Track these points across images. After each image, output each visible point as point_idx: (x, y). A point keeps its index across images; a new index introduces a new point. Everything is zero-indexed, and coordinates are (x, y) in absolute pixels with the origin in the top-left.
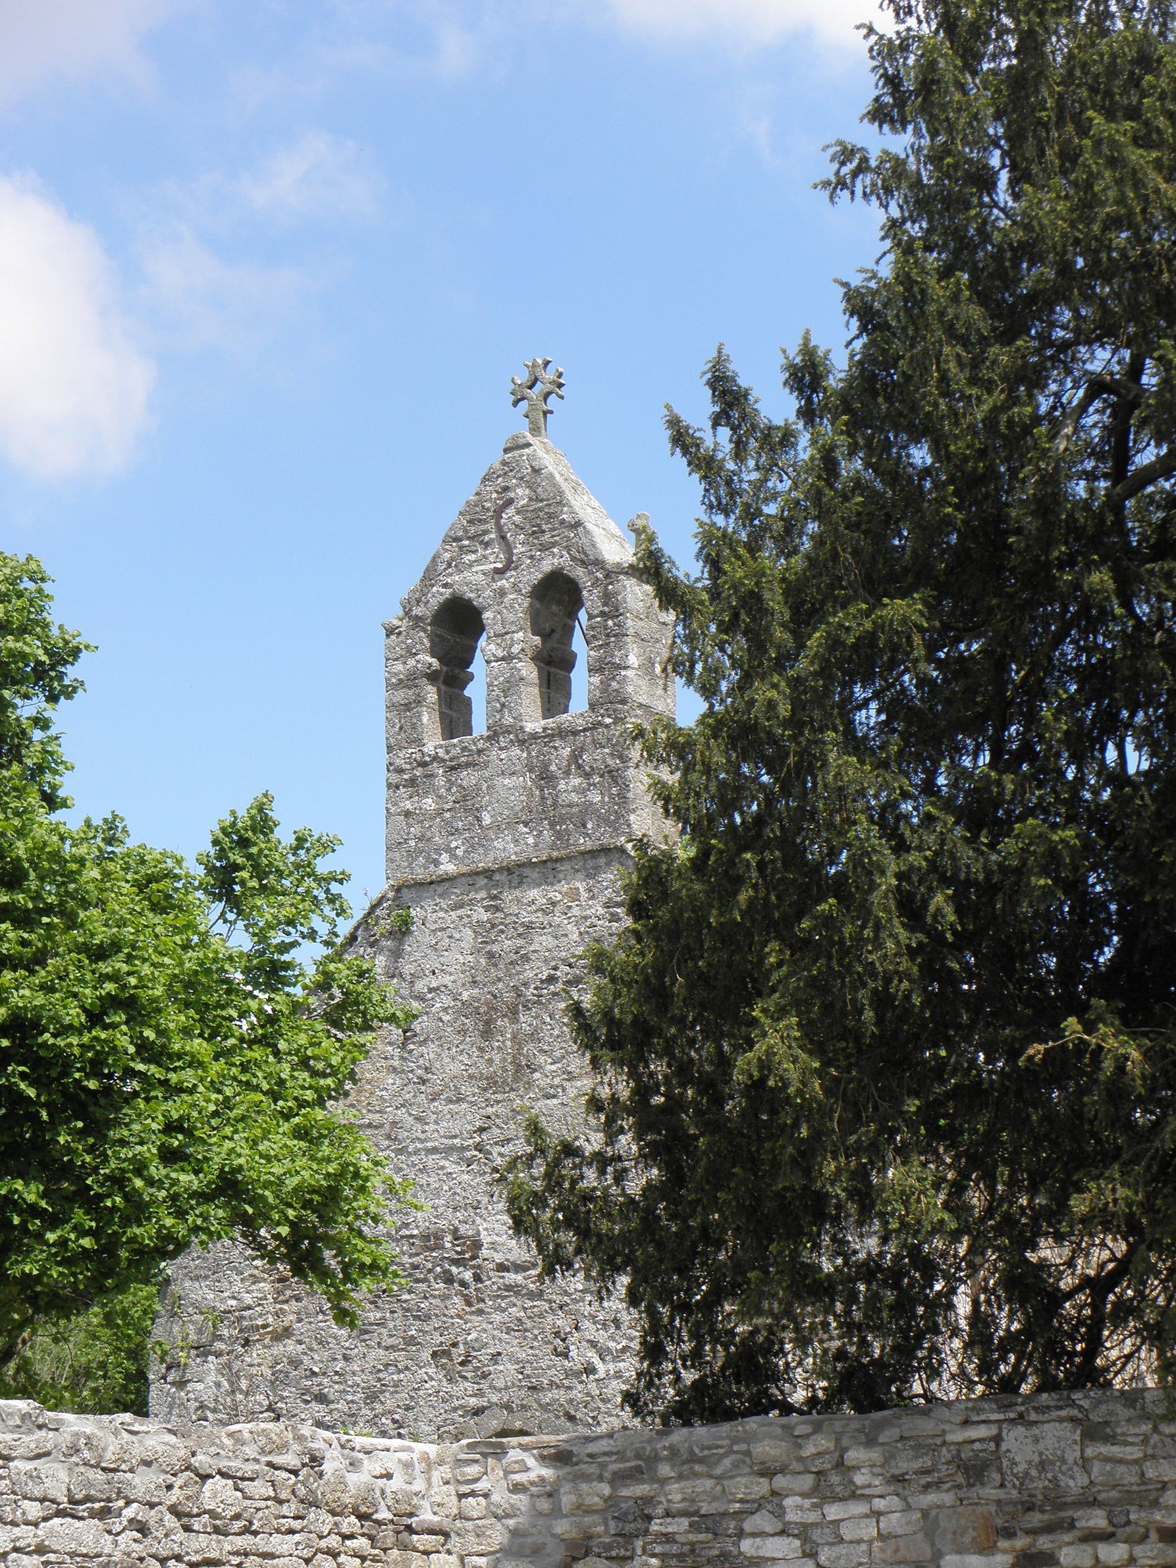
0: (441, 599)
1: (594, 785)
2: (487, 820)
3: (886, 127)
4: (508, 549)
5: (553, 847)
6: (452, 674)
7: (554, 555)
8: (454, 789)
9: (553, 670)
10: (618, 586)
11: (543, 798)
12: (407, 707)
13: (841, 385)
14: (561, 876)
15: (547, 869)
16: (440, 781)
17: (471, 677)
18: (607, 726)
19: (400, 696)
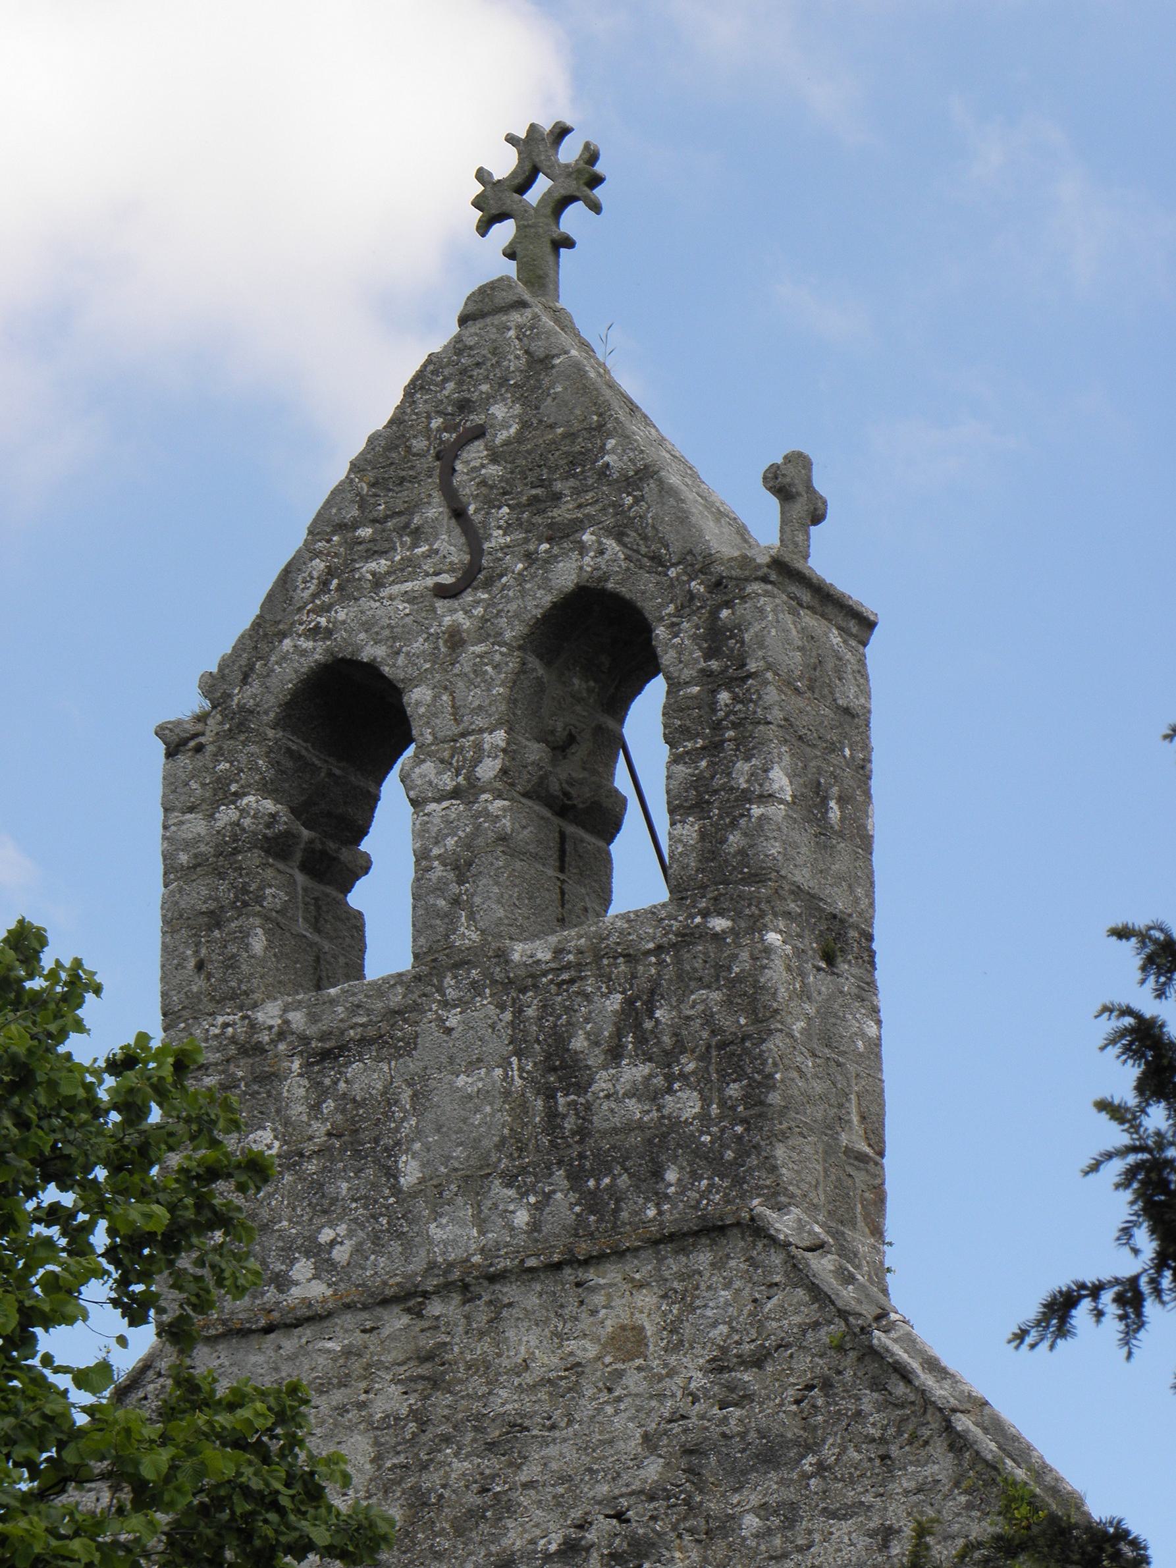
0: (305, 665)
1: (683, 1076)
2: (410, 1172)
3: (1122, 1336)
4: (473, 538)
5: (578, 1229)
6: (327, 850)
7: (582, 549)
8: (329, 1105)
9: (571, 829)
10: (744, 609)
11: (552, 1115)
12: (215, 919)
13: (1140, 1204)
14: (599, 1299)
15: (564, 1265)
16: (295, 1088)
17: (364, 866)
18: (717, 937)
19: (198, 895)
